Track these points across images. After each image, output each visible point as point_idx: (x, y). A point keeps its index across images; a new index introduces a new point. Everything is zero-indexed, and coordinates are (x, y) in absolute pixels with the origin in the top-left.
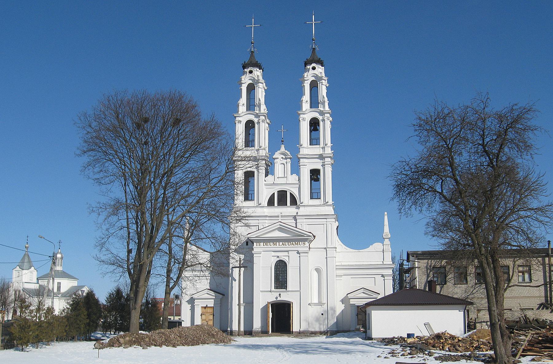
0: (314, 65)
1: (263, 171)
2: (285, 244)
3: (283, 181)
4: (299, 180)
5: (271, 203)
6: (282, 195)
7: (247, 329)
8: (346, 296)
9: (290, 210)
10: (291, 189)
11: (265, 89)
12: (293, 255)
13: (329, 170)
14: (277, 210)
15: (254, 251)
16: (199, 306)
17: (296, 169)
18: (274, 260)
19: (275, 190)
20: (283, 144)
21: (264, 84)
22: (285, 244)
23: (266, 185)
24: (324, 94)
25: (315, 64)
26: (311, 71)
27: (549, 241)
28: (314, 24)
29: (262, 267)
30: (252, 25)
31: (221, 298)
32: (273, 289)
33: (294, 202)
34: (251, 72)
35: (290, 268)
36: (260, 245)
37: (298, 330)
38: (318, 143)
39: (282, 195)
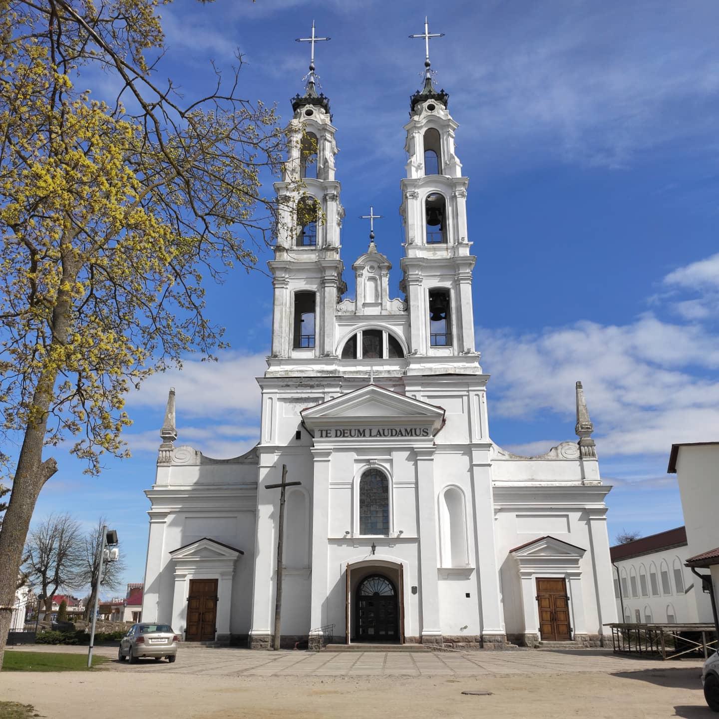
0: (431, 101)
1: (331, 291)
2: (384, 433)
3: (375, 311)
4: (407, 309)
5: (350, 350)
6: (373, 337)
7: (515, 631)
8: (508, 557)
9: (388, 368)
10: (393, 328)
11: (334, 154)
12: (400, 458)
13: (466, 289)
14: (359, 368)
15: (315, 447)
16: (186, 579)
17: (401, 289)
18: (358, 470)
19: (358, 329)
20: (372, 242)
21: (334, 142)
22: (384, 433)
23: (339, 318)
24: (452, 151)
25: (433, 100)
26: (425, 113)
27: (171, 658)
28: (427, 38)
29: (332, 484)
30: (311, 38)
31: (236, 558)
32: (357, 535)
33: (396, 349)
34: (309, 113)
35: (394, 486)
36: (329, 435)
37: (417, 635)
38: (445, 240)
39: (373, 337)
